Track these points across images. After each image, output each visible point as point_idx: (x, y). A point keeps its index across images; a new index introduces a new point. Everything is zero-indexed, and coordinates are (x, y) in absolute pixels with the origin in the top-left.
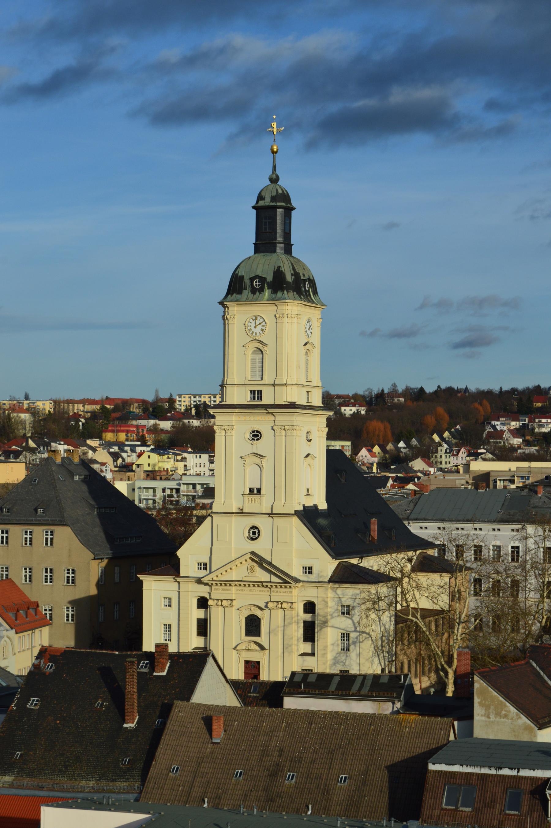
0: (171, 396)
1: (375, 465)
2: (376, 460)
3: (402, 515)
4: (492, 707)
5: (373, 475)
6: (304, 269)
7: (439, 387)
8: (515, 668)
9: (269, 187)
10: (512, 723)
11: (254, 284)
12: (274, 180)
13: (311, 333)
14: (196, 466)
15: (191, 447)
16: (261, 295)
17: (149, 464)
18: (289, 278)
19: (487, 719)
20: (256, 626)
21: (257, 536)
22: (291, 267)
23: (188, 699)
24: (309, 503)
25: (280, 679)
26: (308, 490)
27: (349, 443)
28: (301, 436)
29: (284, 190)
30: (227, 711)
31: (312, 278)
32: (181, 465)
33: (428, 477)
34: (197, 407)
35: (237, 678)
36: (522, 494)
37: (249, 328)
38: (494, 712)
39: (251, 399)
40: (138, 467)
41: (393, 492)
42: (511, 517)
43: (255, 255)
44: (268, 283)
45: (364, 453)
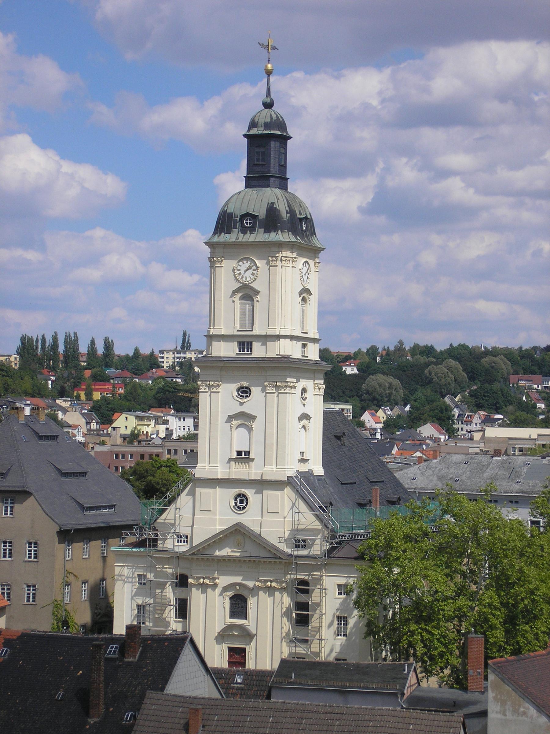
0: (153, 352)
1: (379, 431)
2: (381, 425)
3: (407, 484)
4: (508, 703)
5: (376, 441)
6: (300, 206)
7: (451, 345)
8: (535, 658)
9: (262, 112)
10: (531, 722)
11: (245, 222)
12: (268, 105)
13: (308, 278)
14: (180, 429)
15: (174, 409)
16: (252, 234)
17: (126, 427)
18: (285, 216)
19: (503, 717)
20: (242, 607)
21: (244, 505)
22: (286, 204)
23: (162, 689)
24: (304, 468)
25: (268, 668)
26: (303, 453)
27: (350, 407)
28: (295, 393)
29: (279, 116)
30: (208, 702)
31: (309, 217)
32: (162, 429)
33: (438, 445)
34: (181, 364)
35: (220, 666)
36: (544, 462)
37: (238, 272)
38: (511, 708)
39: (240, 351)
40: (114, 430)
41: (398, 460)
42: (531, 487)
43: (246, 190)
44: (260, 221)
45: (366, 417)
